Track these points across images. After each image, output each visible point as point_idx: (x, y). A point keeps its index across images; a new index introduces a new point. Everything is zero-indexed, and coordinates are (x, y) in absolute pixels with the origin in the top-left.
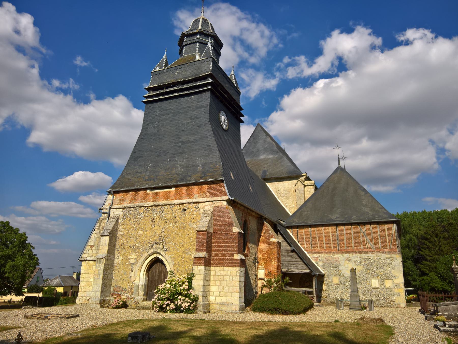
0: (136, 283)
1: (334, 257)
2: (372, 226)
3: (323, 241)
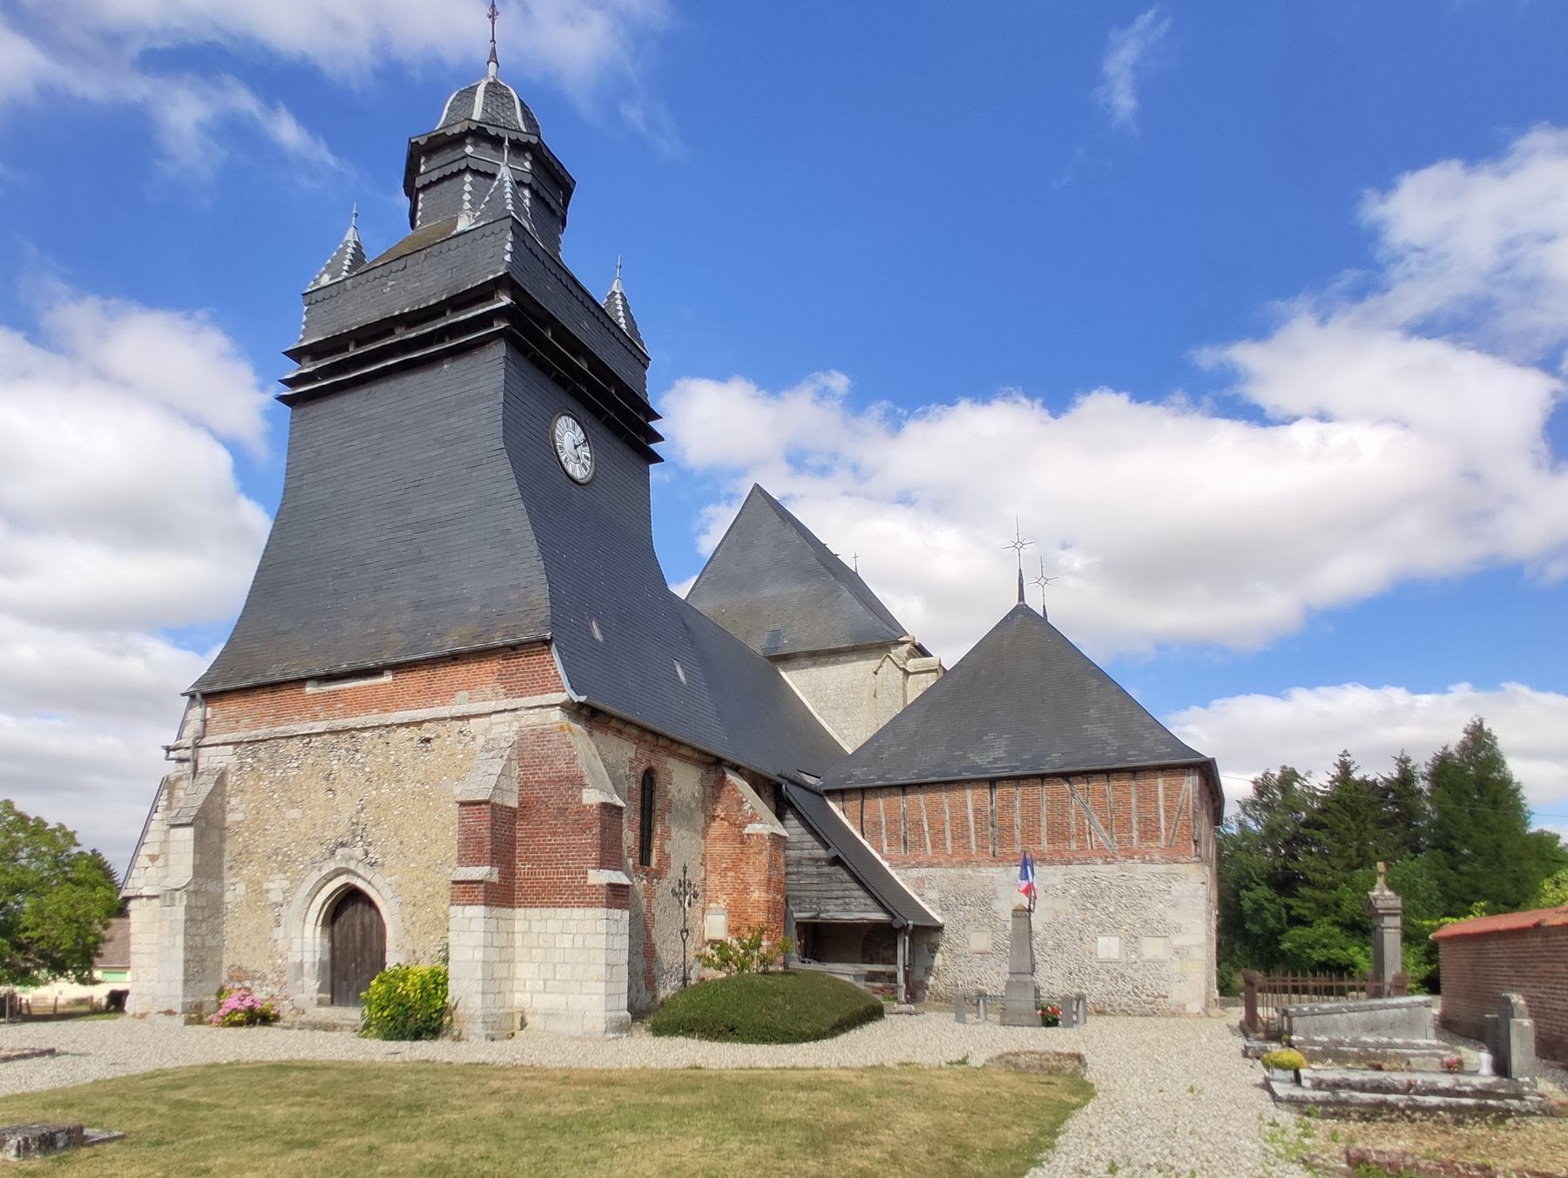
0: (294, 958)
1: (979, 874)
2: (1114, 783)
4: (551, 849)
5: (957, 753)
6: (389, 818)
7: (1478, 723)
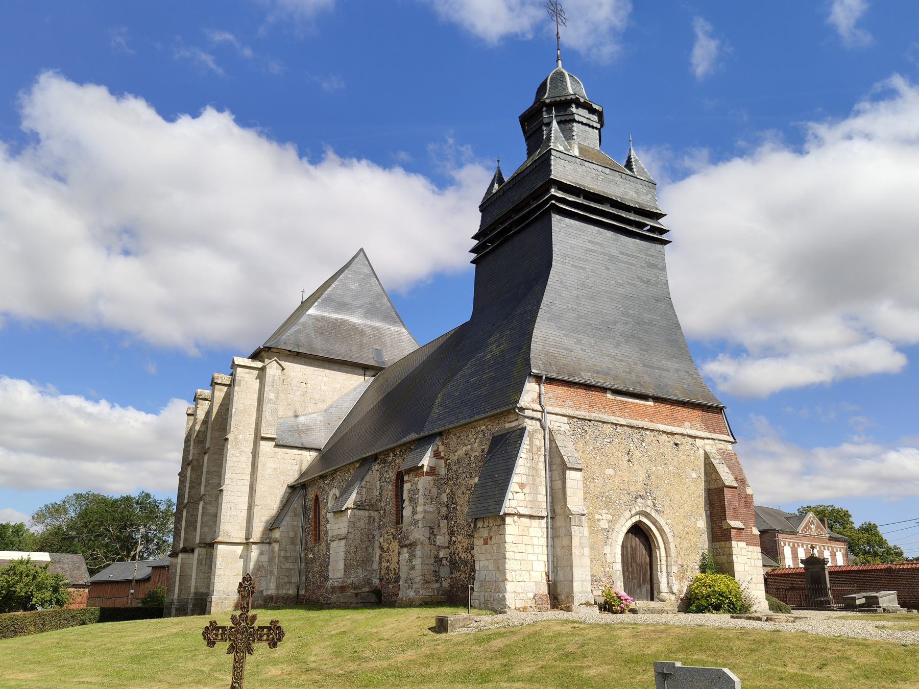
6: (662, 484)
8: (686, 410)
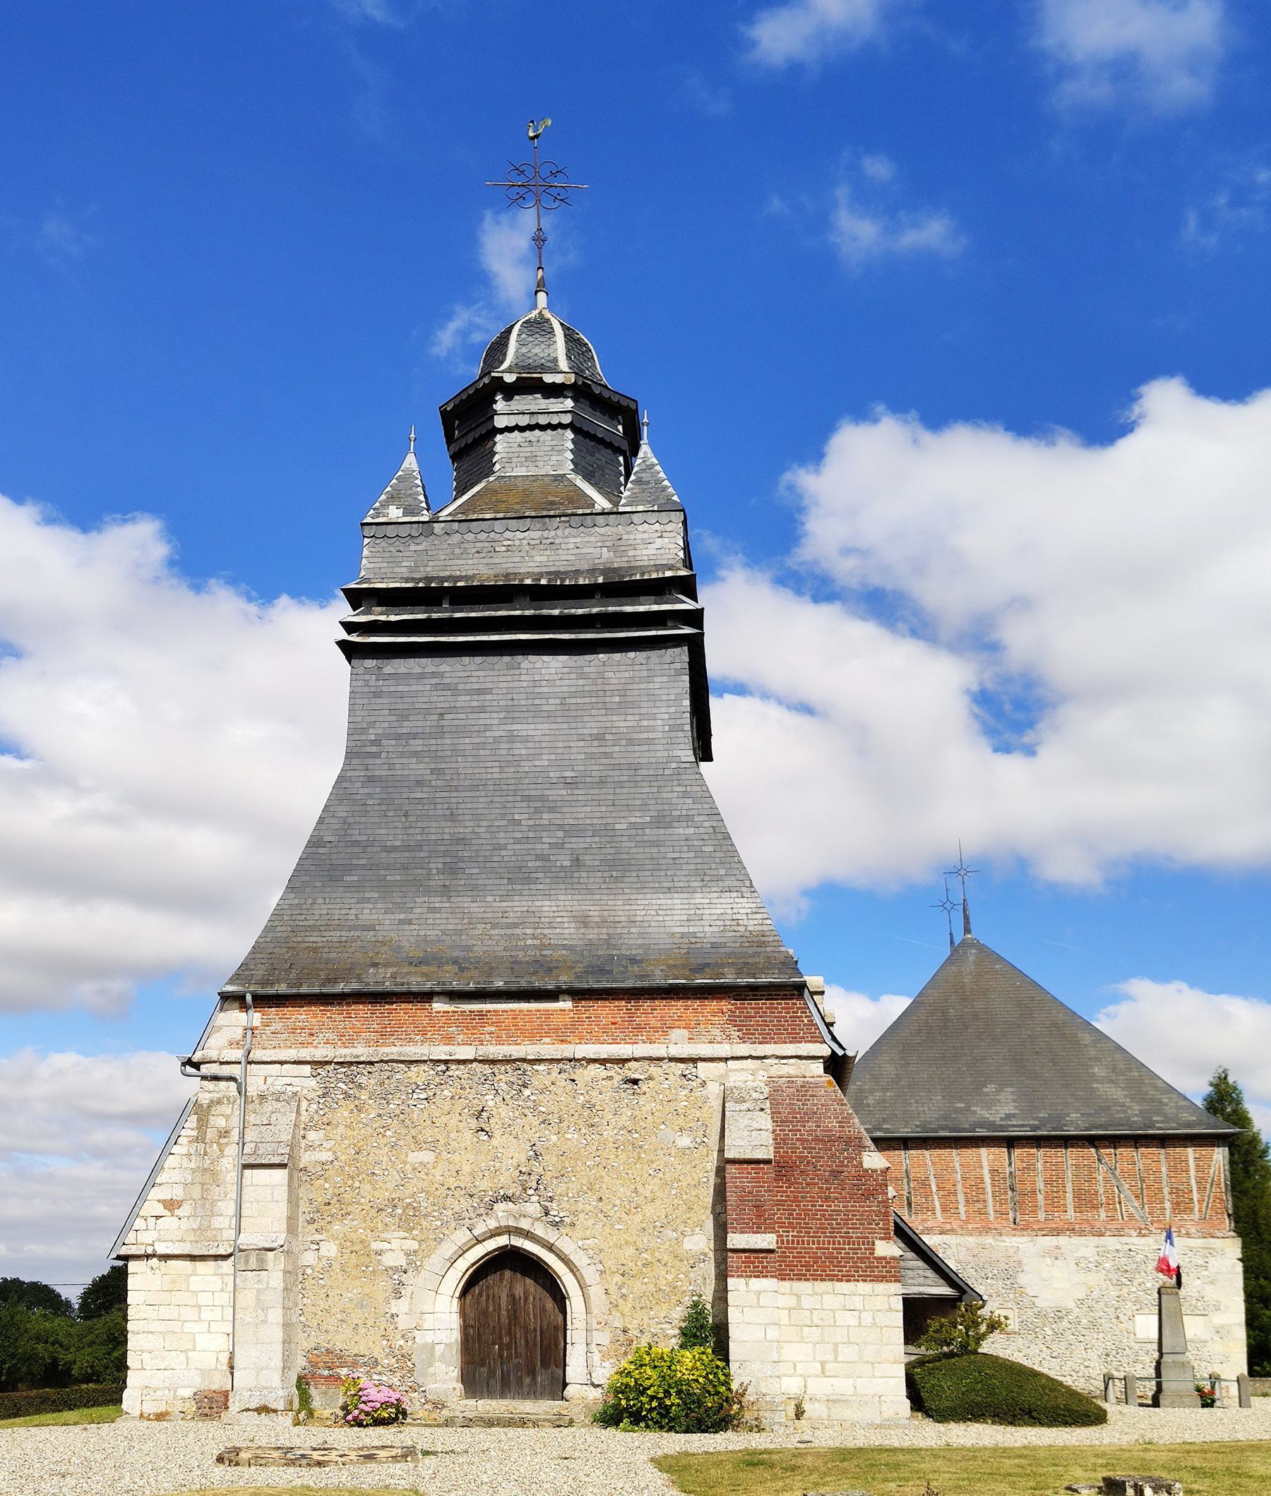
3: (955, 1194)
4: (823, 1215)
5: (959, 1105)
7: (1223, 1075)
8: (680, 1003)
